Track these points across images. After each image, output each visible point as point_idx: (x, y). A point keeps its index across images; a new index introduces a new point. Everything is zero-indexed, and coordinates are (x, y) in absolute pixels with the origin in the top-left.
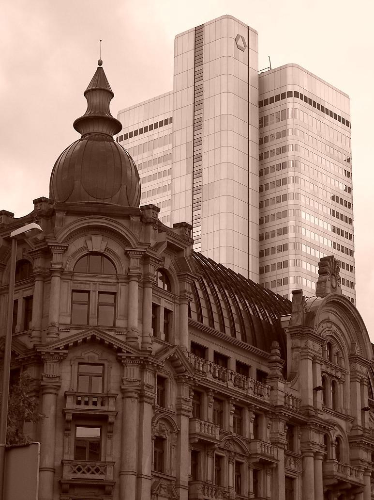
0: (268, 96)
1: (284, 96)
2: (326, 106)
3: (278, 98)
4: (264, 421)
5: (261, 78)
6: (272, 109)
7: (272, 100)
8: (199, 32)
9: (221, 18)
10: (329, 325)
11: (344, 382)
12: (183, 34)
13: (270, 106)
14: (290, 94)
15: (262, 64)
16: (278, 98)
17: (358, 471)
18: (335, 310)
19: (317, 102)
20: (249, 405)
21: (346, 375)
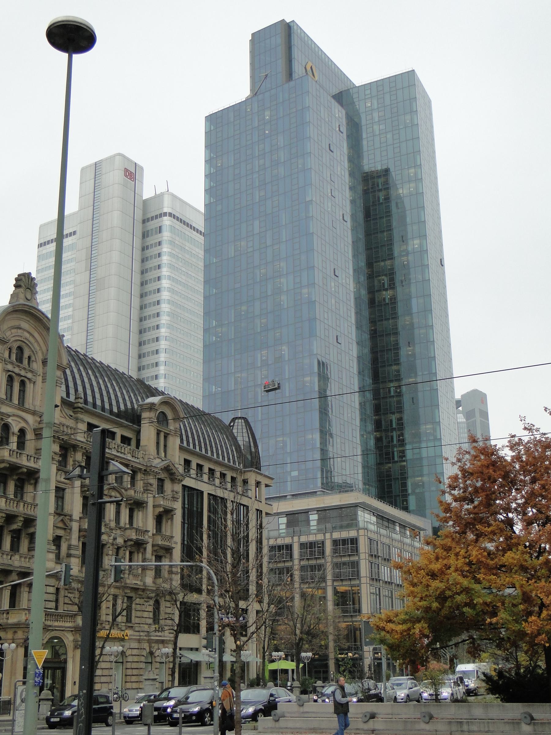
0: (149, 216)
1: (161, 216)
2: (194, 225)
3: (156, 217)
4: (139, 476)
5: (145, 202)
6: (152, 225)
7: (152, 218)
8: (97, 166)
9: (115, 156)
10: (19, 331)
11: (34, 382)
12: (86, 167)
13: (151, 223)
14: (165, 214)
15: (147, 193)
16: (156, 217)
17: (37, 458)
18: (28, 319)
19: (187, 221)
20: (140, 469)
21: (38, 377)
